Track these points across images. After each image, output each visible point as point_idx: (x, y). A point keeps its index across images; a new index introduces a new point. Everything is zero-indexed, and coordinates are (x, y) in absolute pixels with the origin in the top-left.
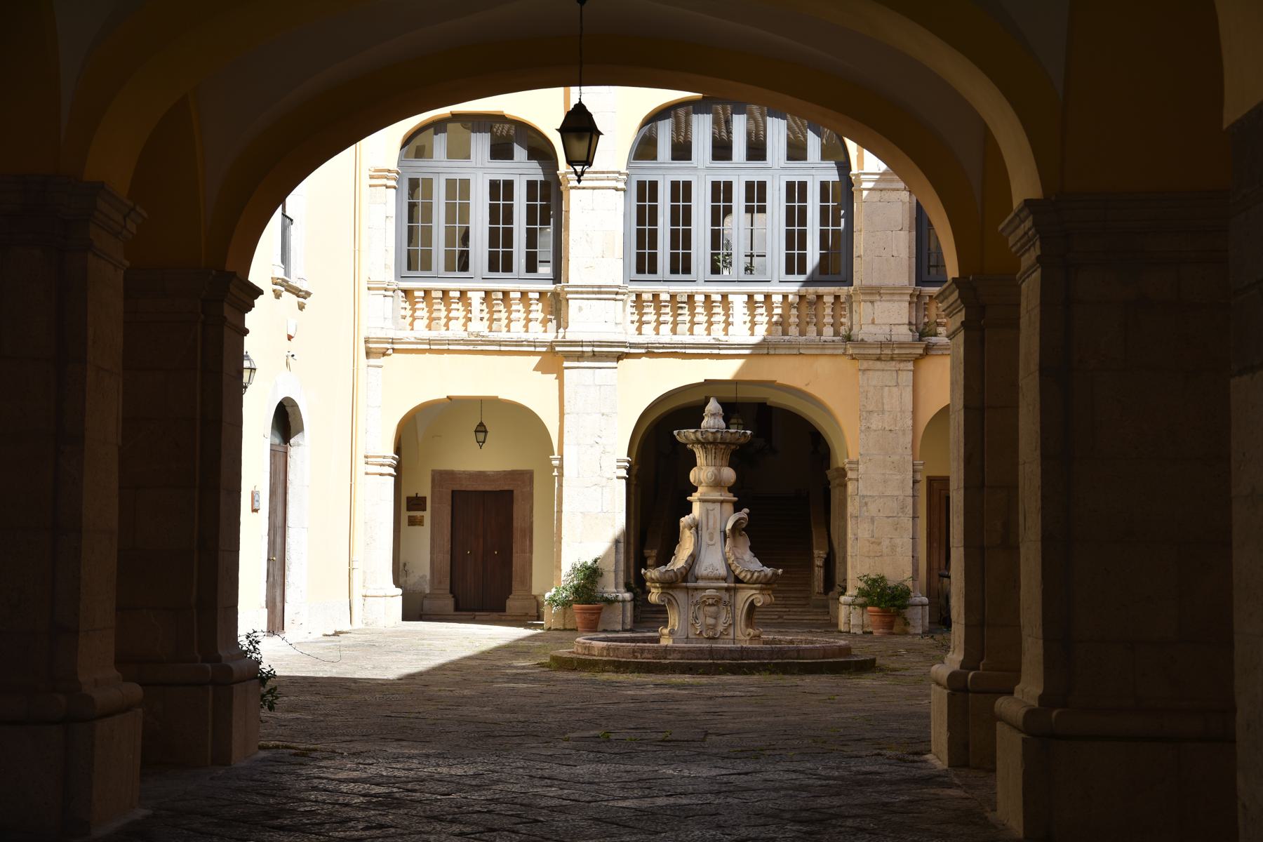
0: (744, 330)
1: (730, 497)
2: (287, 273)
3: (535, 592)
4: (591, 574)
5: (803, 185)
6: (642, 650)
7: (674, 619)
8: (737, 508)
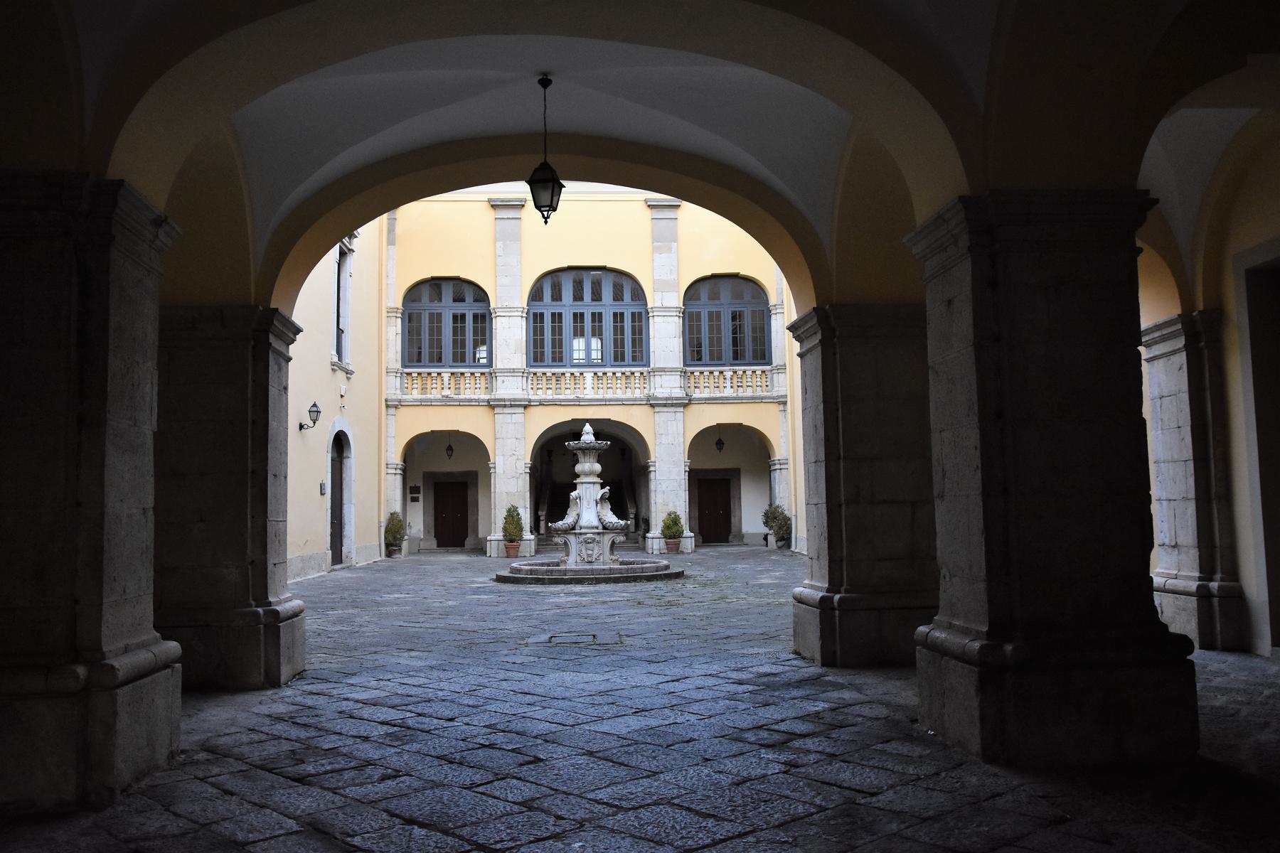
1: (599, 480)
2: (340, 358)
3: (480, 535)
5: (622, 314)
6: (552, 571)
8: (603, 486)
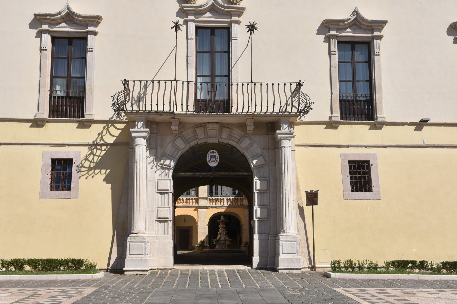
0: (226, 204)
3: (193, 245)
4: (202, 242)
7: (217, 246)
